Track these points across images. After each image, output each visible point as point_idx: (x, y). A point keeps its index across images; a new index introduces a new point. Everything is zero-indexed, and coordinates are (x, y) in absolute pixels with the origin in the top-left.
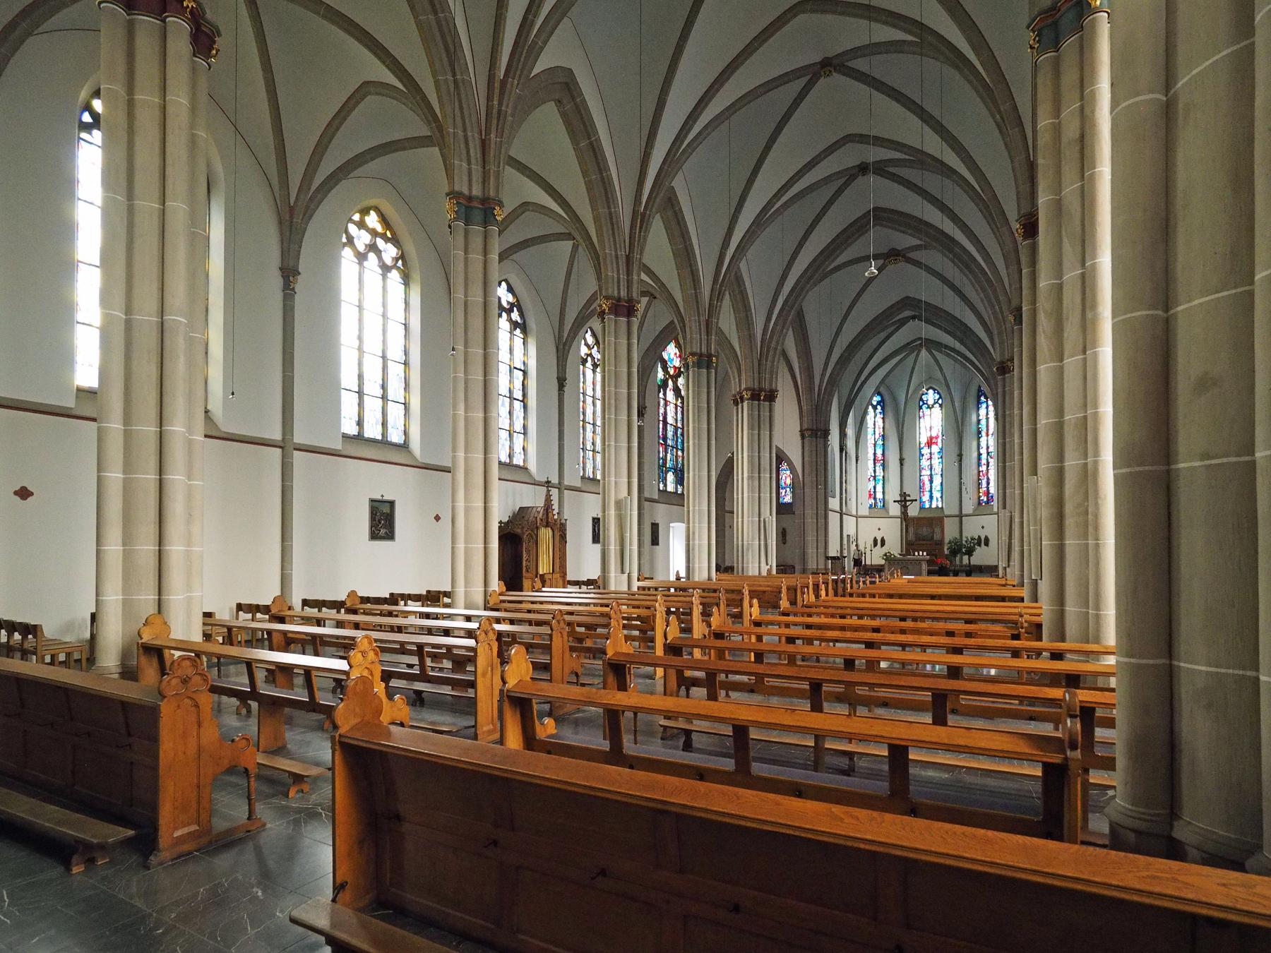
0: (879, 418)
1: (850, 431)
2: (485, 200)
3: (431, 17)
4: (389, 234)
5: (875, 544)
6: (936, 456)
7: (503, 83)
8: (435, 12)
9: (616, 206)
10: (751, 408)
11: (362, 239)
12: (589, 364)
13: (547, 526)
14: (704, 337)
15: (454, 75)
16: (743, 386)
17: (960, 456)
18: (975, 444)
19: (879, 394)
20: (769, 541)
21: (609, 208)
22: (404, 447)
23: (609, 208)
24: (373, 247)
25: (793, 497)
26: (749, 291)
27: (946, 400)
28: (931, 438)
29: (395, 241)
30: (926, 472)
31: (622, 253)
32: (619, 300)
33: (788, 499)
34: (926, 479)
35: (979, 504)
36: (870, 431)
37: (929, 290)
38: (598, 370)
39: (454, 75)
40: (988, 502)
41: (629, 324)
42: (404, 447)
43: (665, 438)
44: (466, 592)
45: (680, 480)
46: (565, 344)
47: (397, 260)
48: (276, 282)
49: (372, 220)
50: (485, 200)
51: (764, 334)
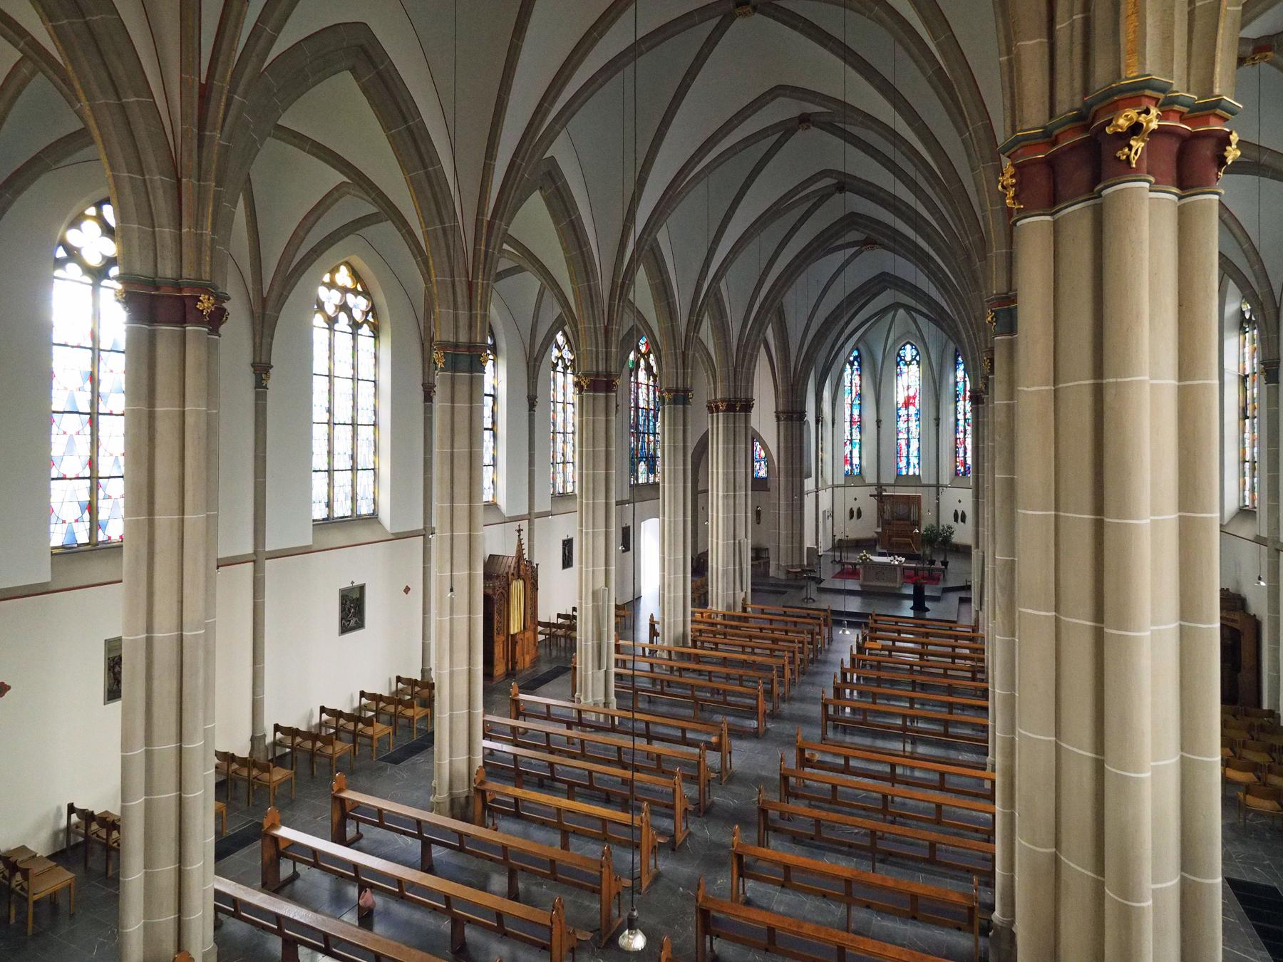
0: (856, 380)
1: (827, 394)
2: (471, 346)
3: (421, 172)
4: (359, 289)
5: (852, 517)
6: (913, 418)
7: (491, 225)
8: (425, 167)
9: (595, 278)
10: (726, 420)
11: (330, 299)
12: (560, 368)
13: (519, 577)
14: (680, 371)
15: (442, 222)
16: (719, 396)
17: (937, 420)
18: (952, 407)
19: (858, 350)
20: (744, 566)
21: (588, 280)
22: (373, 517)
23: (588, 280)
24: (344, 307)
25: (768, 472)
26: (725, 298)
27: (923, 358)
28: (909, 398)
29: (366, 293)
30: (903, 436)
31: (600, 326)
32: (597, 375)
33: (762, 473)
34: (903, 443)
35: (957, 474)
36: (847, 389)
37: (906, 270)
38: (569, 371)
39: (442, 222)
40: (964, 474)
41: (607, 398)
42: (373, 517)
43: (637, 425)
44: (451, 763)
45: (651, 469)
46: (536, 360)
47: (367, 313)
48: (248, 378)
49: (343, 277)
50: (471, 346)
51: (740, 340)
